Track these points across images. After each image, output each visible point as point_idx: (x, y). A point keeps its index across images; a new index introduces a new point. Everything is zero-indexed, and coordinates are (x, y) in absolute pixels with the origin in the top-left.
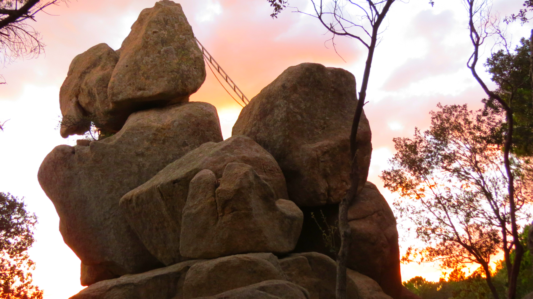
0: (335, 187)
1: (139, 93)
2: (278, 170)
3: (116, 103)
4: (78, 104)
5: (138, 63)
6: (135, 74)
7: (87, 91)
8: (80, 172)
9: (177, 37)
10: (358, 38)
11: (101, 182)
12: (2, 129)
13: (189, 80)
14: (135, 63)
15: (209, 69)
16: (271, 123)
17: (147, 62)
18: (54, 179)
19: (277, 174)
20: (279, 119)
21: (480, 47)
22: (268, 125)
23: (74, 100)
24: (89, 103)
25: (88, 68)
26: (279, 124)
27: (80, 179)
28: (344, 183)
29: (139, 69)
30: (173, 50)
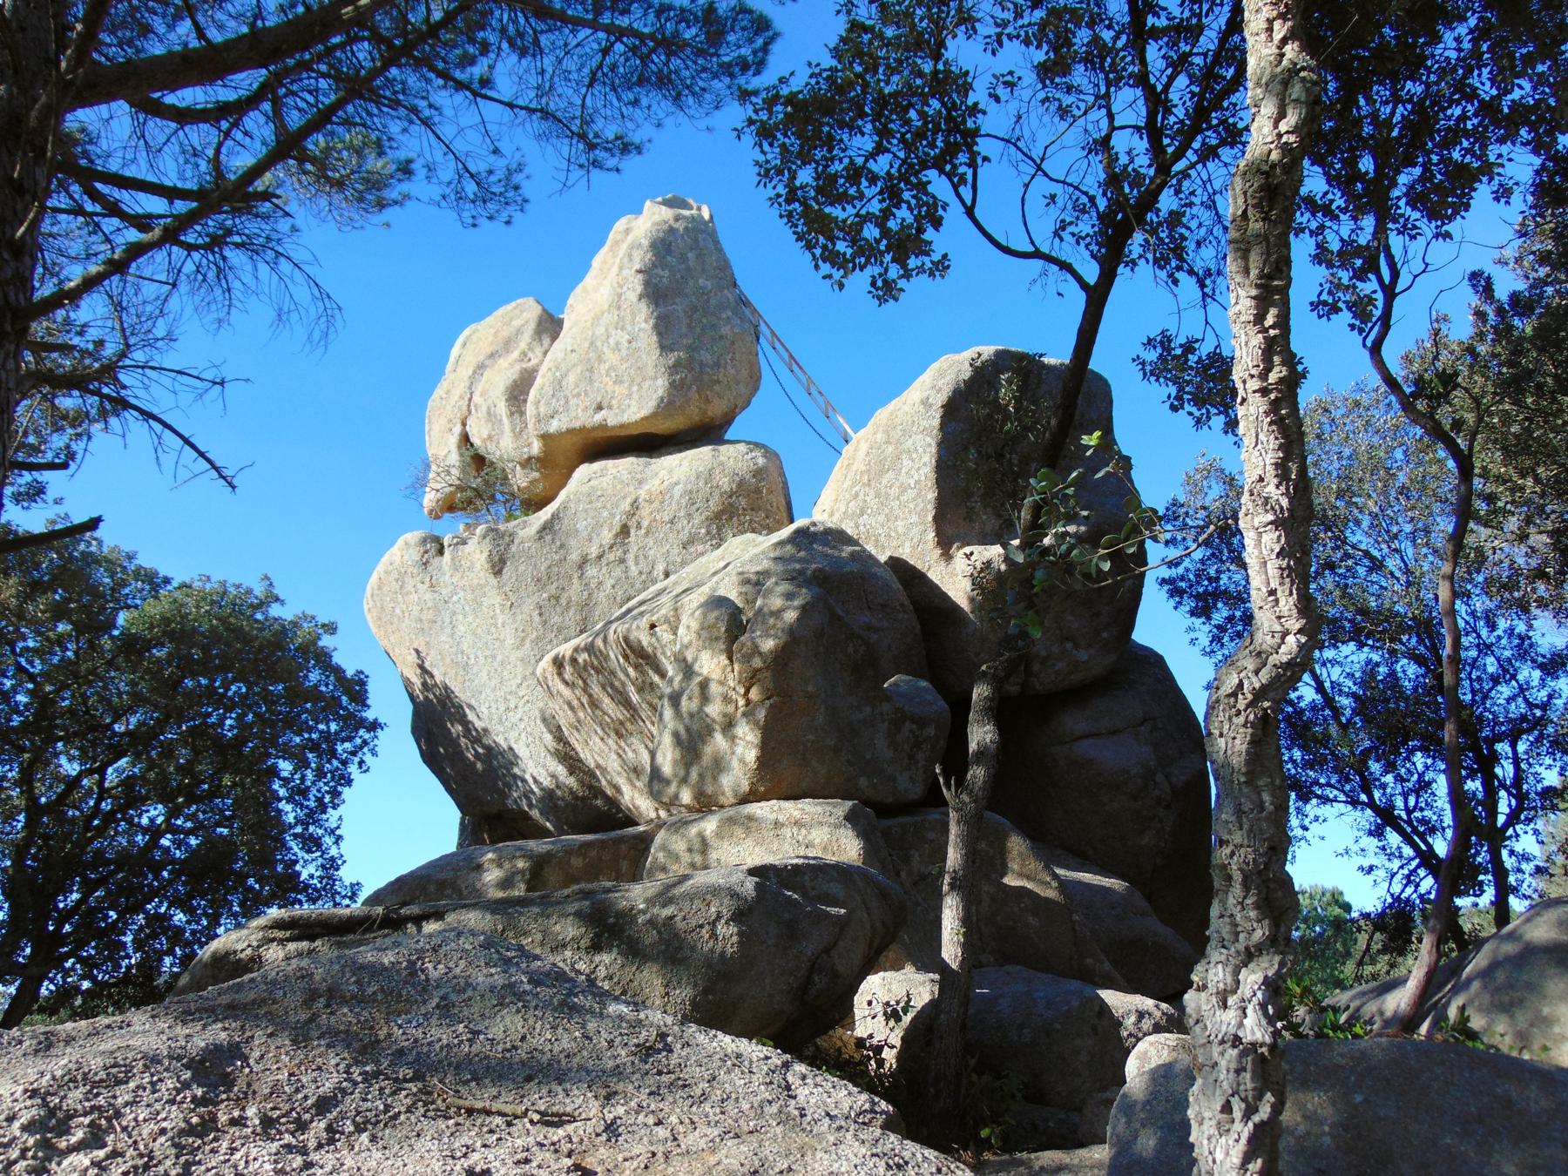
0: (1044, 653)
1: (598, 417)
2: (902, 605)
3: (545, 437)
4: (465, 439)
5: (599, 344)
6: (591, 370)
7: (484, 409)
8: (455, 598)
9: (691, 283)
10: (1006, 250)
11: (500, 622)
12: (234, 487)
13: (717, 388)
14: (592, 343)
15: (770, 360)
16: (893, 492)
17: (618, 344)
18: (398, 611)
19: (900, 616)
20: (912, 482)
21: (1397, 302)
22: (887, 496)
23: (458, 429)
24: (490, 437)
25: (492, 356)
26: (911, 494)
27: (455, 613)
28: (1069, 646)
29: (600, 359)
30: (681, 315)
